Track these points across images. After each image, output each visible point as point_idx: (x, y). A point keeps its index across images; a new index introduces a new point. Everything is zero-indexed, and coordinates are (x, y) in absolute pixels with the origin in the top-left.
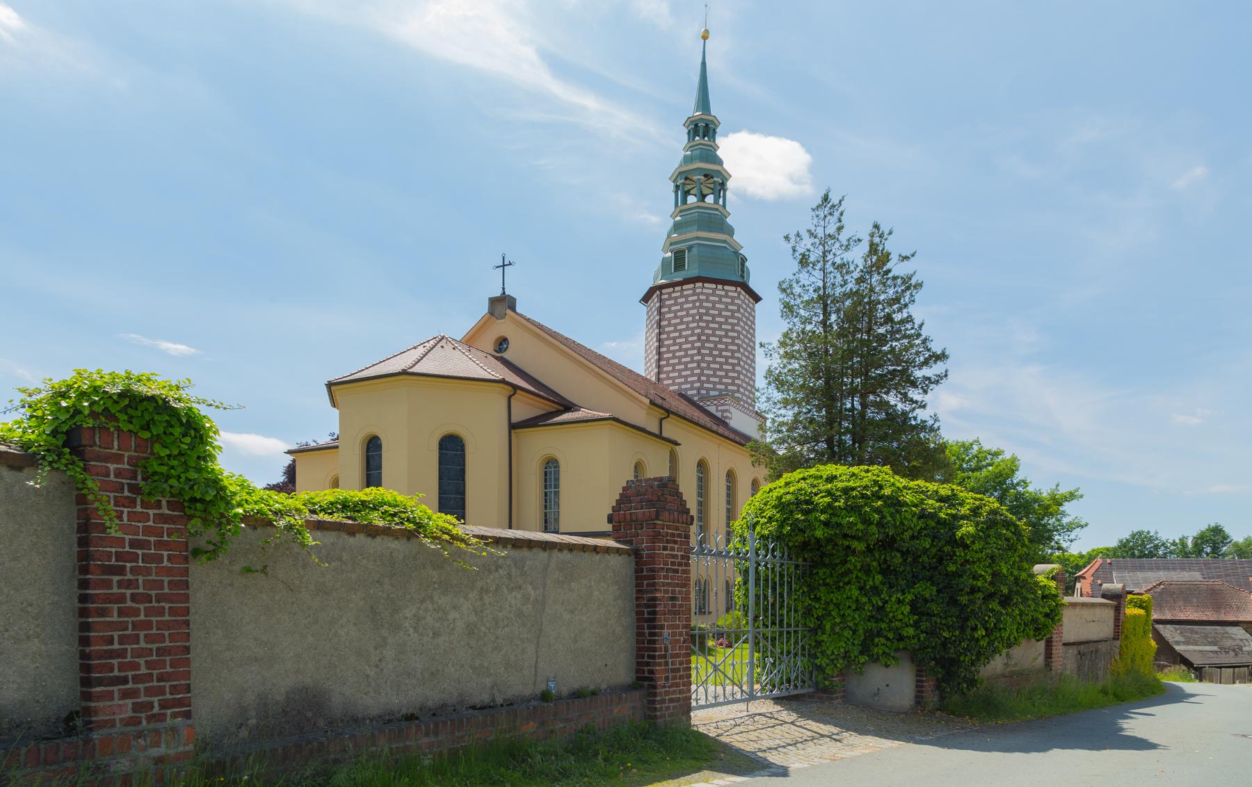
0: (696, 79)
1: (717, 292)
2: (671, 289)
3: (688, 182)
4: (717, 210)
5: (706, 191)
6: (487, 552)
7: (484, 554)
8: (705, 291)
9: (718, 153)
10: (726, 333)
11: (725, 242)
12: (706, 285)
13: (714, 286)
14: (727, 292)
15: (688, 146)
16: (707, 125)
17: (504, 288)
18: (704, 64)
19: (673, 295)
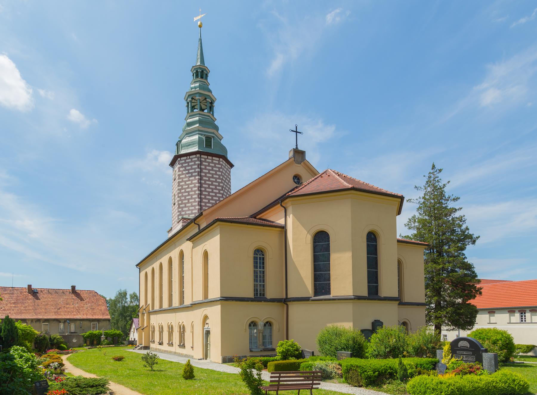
0: (197, 44)
1: (207, 160)
2: (186, 158)
3: (193, 101)
4: (209, 116)
5: (203, 107)
6: (8, 362)
7: (7, 363)
9: (222, 142)
10: (209, 194)
11: (213, 133)
15: (193, 82)
16: (202, 71)
17: (297, 145)
19: (187, 161)
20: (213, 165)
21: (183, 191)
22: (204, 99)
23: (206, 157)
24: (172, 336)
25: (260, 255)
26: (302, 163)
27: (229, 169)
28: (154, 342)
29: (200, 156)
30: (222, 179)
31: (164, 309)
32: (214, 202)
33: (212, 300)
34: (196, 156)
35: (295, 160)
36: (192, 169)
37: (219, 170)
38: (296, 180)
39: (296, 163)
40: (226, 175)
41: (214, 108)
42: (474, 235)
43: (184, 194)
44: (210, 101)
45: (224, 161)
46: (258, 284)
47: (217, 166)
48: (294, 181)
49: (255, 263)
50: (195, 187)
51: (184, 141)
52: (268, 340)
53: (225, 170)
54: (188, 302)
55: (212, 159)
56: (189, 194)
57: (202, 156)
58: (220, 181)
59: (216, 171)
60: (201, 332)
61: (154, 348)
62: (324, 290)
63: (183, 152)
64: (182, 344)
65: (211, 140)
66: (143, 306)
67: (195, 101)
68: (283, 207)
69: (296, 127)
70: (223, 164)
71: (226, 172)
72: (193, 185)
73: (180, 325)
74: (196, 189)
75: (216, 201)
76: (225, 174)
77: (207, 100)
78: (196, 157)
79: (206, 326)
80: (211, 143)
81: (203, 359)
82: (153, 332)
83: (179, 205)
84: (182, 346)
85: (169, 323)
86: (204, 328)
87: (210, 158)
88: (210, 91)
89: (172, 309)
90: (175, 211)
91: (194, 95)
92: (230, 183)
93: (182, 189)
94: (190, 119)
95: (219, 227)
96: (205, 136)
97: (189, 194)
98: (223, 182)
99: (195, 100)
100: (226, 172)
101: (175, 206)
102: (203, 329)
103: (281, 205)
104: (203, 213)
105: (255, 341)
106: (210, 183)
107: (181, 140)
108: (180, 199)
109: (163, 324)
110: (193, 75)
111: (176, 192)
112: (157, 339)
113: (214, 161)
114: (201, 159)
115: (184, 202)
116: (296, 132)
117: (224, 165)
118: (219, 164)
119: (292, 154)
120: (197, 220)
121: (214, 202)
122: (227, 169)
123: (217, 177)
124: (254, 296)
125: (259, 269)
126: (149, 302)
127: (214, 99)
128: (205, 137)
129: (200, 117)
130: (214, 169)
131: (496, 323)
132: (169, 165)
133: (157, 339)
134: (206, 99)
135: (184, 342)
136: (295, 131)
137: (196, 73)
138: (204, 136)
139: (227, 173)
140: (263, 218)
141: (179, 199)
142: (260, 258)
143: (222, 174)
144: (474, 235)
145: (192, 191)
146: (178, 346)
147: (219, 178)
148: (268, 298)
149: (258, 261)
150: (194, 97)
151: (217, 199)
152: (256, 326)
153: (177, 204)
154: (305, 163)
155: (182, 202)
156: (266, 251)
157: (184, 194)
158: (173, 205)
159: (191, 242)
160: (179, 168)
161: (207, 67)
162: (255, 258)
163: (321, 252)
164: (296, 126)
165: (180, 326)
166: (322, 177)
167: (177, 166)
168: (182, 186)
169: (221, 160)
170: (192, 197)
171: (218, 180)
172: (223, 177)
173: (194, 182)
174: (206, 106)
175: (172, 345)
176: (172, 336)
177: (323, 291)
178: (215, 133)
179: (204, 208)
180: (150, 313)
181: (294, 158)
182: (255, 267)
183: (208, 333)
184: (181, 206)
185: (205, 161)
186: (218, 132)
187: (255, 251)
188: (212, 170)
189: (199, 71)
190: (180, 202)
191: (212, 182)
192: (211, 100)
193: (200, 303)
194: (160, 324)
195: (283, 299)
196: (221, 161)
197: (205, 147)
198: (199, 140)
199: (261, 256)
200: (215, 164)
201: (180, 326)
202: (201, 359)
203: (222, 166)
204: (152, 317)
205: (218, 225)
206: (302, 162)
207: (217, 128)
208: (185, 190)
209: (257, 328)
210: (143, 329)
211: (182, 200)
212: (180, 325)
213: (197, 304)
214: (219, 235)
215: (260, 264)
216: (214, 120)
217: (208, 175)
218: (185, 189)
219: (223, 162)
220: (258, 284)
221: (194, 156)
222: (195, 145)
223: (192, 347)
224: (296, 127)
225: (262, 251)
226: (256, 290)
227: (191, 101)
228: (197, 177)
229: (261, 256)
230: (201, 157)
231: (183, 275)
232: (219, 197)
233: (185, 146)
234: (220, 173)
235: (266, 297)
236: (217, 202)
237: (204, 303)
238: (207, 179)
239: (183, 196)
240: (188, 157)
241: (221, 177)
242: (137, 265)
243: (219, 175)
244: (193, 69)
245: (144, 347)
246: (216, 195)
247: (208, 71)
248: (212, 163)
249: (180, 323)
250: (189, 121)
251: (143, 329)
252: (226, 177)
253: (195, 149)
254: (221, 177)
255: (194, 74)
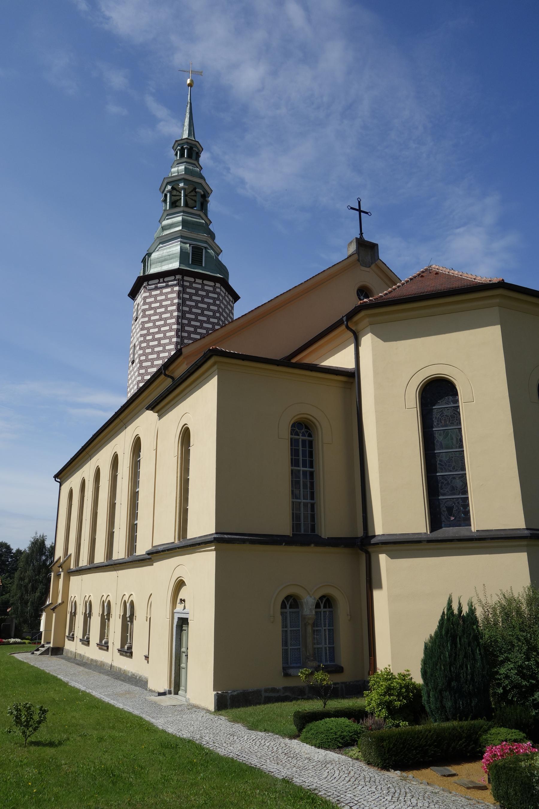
1: (194, 285)
2: (157, 281)
11: (206, 242)
17: (361, 234)
20: (204, 293)
21: (149, 338)
22: (192, 189)
23: (192, 280)
24: (108, 627)
25: (303, 435)
26: (373, 266)
27: (231, 303)
28: (73, 638)
29: (183, 277)
30: (219, 306)
31: (96, 565)
32: (204, 331)
33: (196, 540)
34: (175, 277)
35: (360, 259)
36: (166, 300)
37: (214, 302)
39: (361, 265)
40: (226, 313)
41: (208, 205)
43: (151, 344)
44: (203, 193)
45: (222, 288)
46: (300, 503)
47: (211, 295)
49: (294, 452)
50: (171, 330)
51: (154, 256)
52: (326, 644)
53: (223, 316)
54: (142, 549)
55: (203, 283)
57: (186, 278)
58: (216, 321)
59: (209, 304)
60: (167, 622)
61: (71, 652)
62: (453, 516)
63: (153, 270)
64: (126, 647)
65: (202, 253)
66: (60, 558)
67: (178, 192)
68: (351, 330)
69: (359, 203)
70: (222, 293)
71: (226, 307)
72: (167, 328)
73: (104, 600)
74: (173, 333)
75: (207, 329)
76: (224, 310)
77: (197, 190)
78: (175, 279)
79: (179, 607)
80: (202, 257)
81: (170, 693)
82: (73, 615)
83: (141, 362)
84: (125, 652)
85: (103, 596)
86: (175, 611)
87: (200, 281)
88: (202, 178)
89: (112, 565)
90: (134, 374)
91: (176, 183)
92: (233, 315)
93: (149, 334)
94: (167, 219)
95: (215, 367)
97: (159, 343)
98: (221, 323)
99: (177, 191)
100: (226, 307)
101: (134, 365)
102: (173, 613)
103: (348, 327)
104: (183, 350)
105: (294, 647)
106: (198, 324)
107: (151, 253)
108: (144, 352)
109: (92, 599)
111: (138, 339)
112: (79, 633)
113: (206, 288)
114: (183, 283)
115: (150, 357)
116: (360, 211)
117: (223, 295)
118: (214, 292)
119: (353, 248)
120: (171, 368)
121: (204, 331)
122: (228, 303)
123: (211, 314)
124: (293, 531)
125: (303, 467)
126: (72, 550)
127: (209, 192)
128: (191, 247)
129: (184, 217)
130: (206, 300)
131: (151, 595)
133: (79, 633)
134: (195, 189)
135: (131, 643)
136: (358, 209)
137: (180, 150)
138: (190, 246)
139: (228, 309)
140: (307, 361)
141: (141, 352)
142: (304, 441)
143: (218, 309)
145: (165, 337)
146: (119, 650)
147: (214, 317)
148: (323, 537)
149: (301, 448)
150: (175, 187)
151: (210, 326)
152: (298, 607)
153: (137, 361)
154: (377, 266)
155: (147, 357)
156: (315, 426)
157: (151, 344)
158: (130, 364)
159: (156, 412)
160: (145, 298)
161: (198, 142)
162: (294, 443)
163: (439, 427)
164: (359, 200)
165: (125, 603)
166: (422, 276)
168: (148, 329)
169: (218, 285)
170: (164, 348)
171: (212, 320)
172: (221, 314)
173: (169, 321)
174: (195, 201)
175: (106, 648)
176: (108, 627)
177: (452, 518)
178: (208, 241)
179: (186, 341)
180: (70, 573)
181: (359, 255)
182: (294, 462)
183: (183, 622)
184: (145, 364)
185: (191, 287)
186: (214, 241)
187: (293, 425)
188: (202, 302)
189: (186, 147)
190: (143, 358)
191: (202, 322)
192: (203, 191)
193: (168, 550)
194: (104, 598)
195: (357, 538)
196: (218, 288)
198: (180, 251)
199: (306, 438)
200: (208, 292)
201: (125, 603)
202: (164, 694)
203: (218, 297)
204: (74, 580)
205: (215, 363)
206: (372, 264)
207: (212, 235)
208: (153, 337)
209: (300, 613)
210: (53, 609)
211: (147, 355)
212: (104, 600)
213: (163, 551)
214: (217, 376)
215: (304, 455)
217: (194, 310)
218: (154, 334)
219: (221, 290)
220: (300, 503)
221: (172, 278)
222: (174, 260)
223: (147, 658)
224: (359, 203)
225: (307, 427)
226: (296, 517)
227: (170, 192)
228: (176, 288)
229: (306, 438)
230: (183, 280)
231: (137, 490)
232: (213, 324)
233: (157, 263)
234: (216, 308)
235: (320, 535)
236: (210, 332)
237: (177, 550)
238: (193, 317)
239: (148, 347)
240: (161, 280)
241: (218, 315)
242: (56, 476)
243: (214, 312)
244: (176, 144)
245: (53, 649)
246: (208, 320)
247: (201, 149)
248: (203, 289)
249: (126, 598)
250: (165, 223)
251: (53, 609)
252: (225, 315)
253: (175, 265)
254: (218, 302)
255: (177, 152)
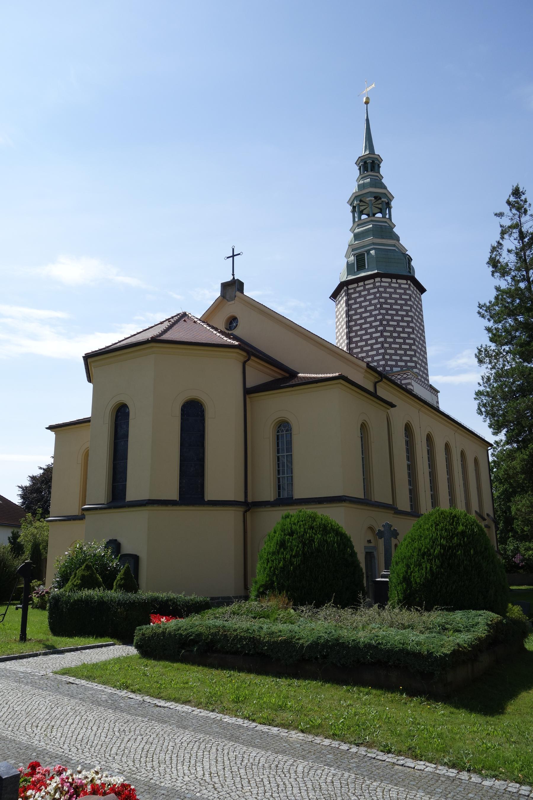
2: (356, 285)
3: (362, 204)
8: (383, 284)
12: (383, 279)
13: (389, 280)
14: (400, 284)
15: (360, 177)
16: (373, 162)
18: (367, 120)
19: (358, 289)
34: (375, 280)
38: (235, 324)
42: (474, 398)
48: (237, 325)
56: (371, 336)
69: (239, 254)
96: (355, 256)
110: (360, 169)
132: (330, 298)
144: (474, 398)
167: (343, 299)
197: (356, 271)
216: (391, 227)
224: (239, 254)
